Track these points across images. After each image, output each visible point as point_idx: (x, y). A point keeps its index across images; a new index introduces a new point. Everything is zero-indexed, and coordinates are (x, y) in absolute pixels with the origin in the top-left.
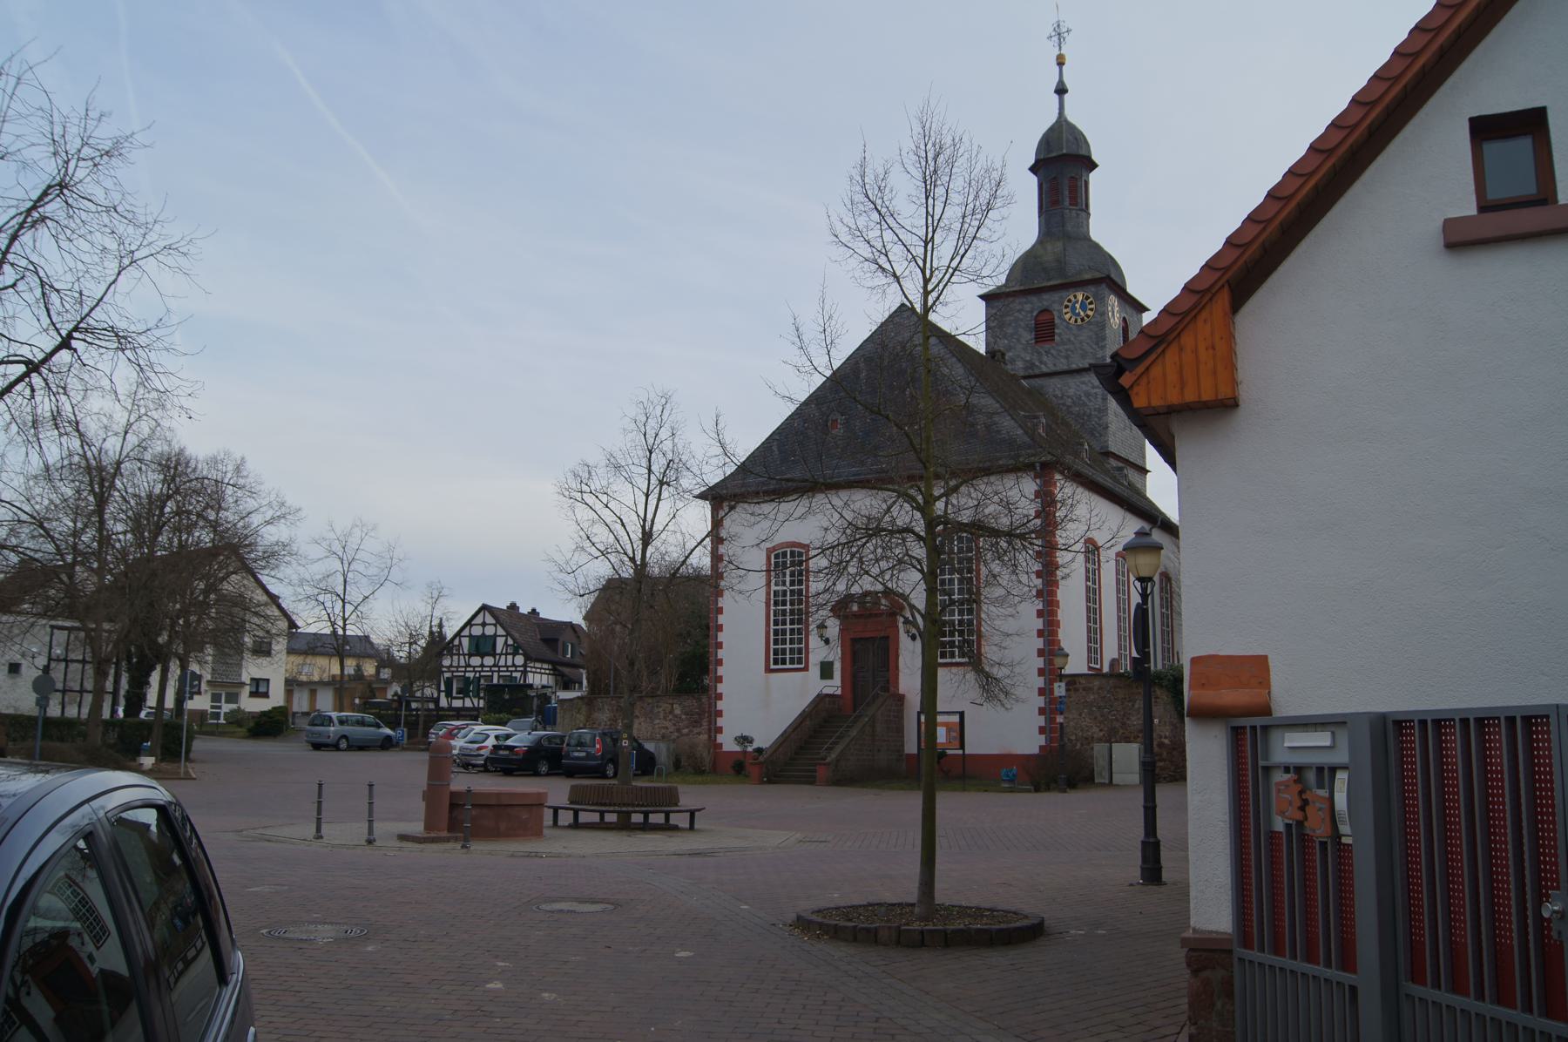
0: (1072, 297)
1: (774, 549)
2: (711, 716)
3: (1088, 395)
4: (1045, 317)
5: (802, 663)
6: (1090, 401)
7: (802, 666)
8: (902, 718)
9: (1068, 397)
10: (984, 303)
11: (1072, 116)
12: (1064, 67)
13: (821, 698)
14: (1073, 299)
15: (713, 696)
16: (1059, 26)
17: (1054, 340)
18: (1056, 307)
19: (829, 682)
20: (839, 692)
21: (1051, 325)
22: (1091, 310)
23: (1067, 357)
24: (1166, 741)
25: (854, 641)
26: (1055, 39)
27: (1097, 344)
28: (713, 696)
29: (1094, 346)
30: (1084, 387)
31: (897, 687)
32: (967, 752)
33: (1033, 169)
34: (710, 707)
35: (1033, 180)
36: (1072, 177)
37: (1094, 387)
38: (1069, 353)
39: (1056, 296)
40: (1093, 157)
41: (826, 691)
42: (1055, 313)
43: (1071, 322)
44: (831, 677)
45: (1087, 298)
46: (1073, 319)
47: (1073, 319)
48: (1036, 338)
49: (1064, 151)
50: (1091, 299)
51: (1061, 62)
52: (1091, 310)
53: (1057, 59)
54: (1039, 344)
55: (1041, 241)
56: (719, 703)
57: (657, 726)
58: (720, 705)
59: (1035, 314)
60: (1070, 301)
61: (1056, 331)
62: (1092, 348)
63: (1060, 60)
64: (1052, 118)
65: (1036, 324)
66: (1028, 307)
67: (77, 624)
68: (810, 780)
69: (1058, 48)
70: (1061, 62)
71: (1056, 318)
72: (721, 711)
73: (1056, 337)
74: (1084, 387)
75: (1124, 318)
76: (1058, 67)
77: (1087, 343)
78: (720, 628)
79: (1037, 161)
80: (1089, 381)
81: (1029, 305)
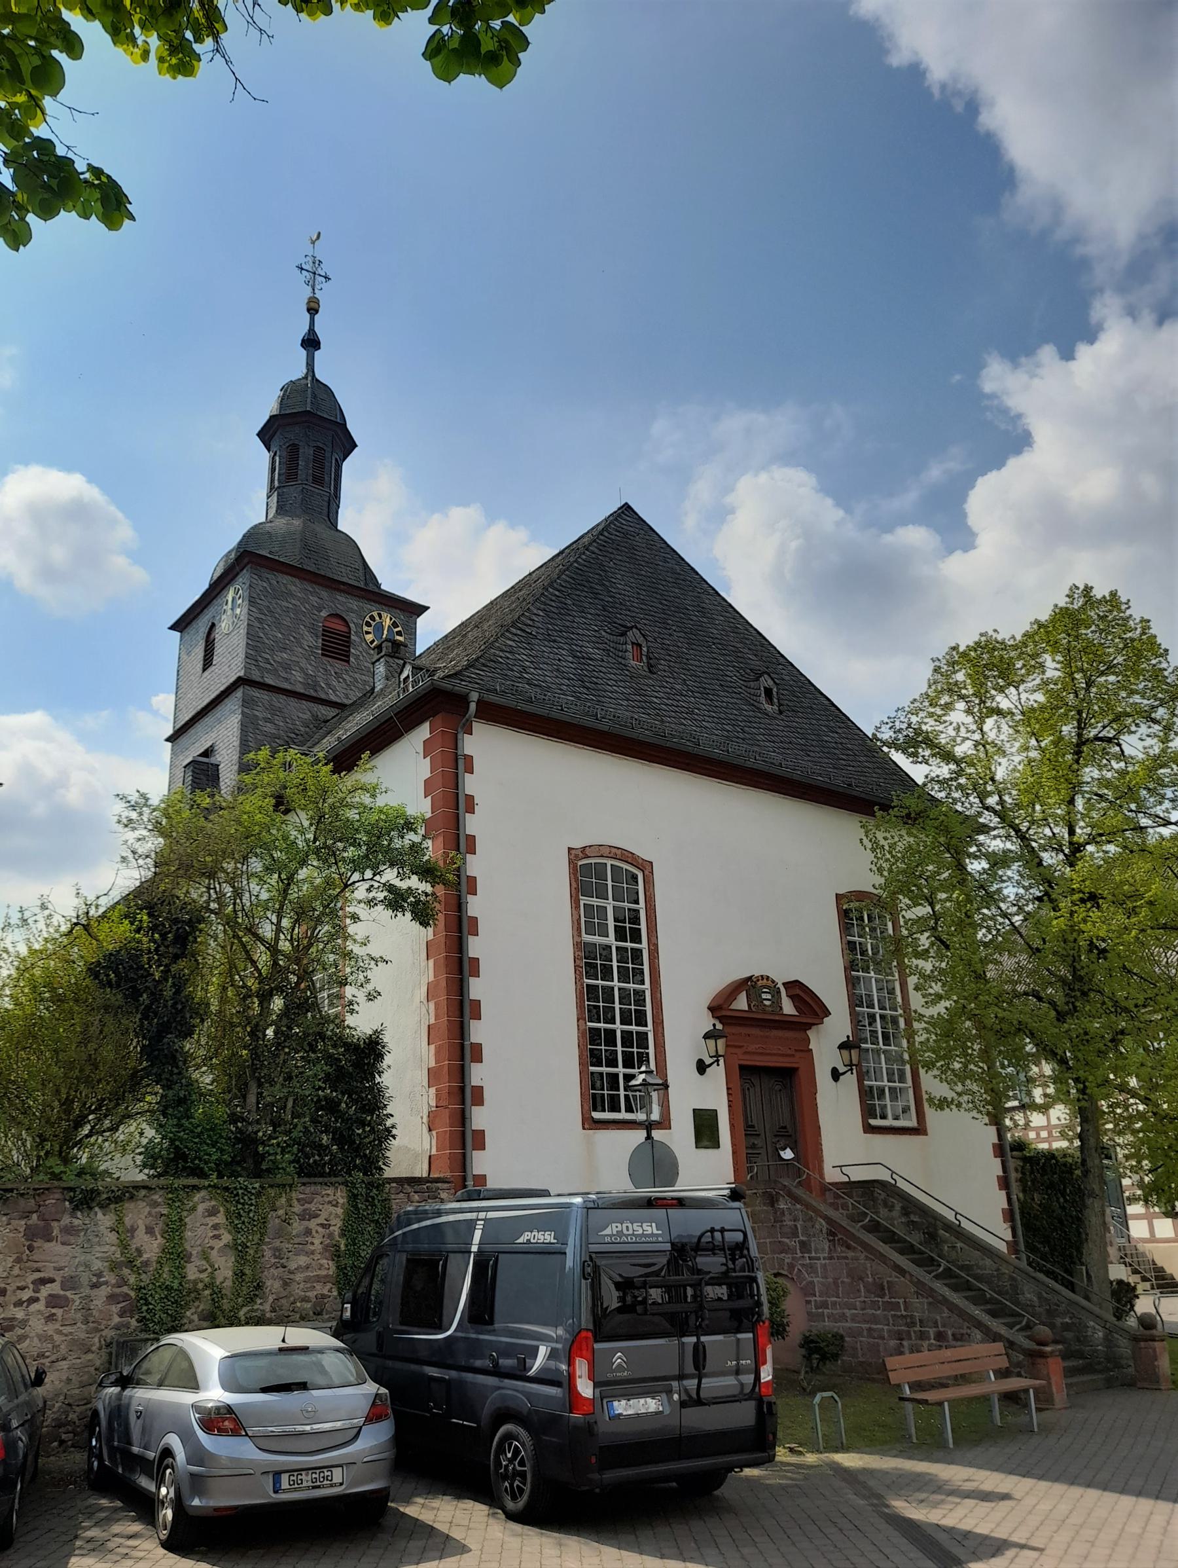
0: (375, 614)
4: (339, 627)
12: (316, 317)
14: (377, 618)
25: (742, 1068)
33: (267, 434)
42: (352, 625)
44: (716, 1144)
50: (399, 629)
51: (313, 309)
53: (309, 303)
57: (299, 1277)
60: (372, 618)
63: (312, 305)
70: (313, 309)
76: (308, 316)
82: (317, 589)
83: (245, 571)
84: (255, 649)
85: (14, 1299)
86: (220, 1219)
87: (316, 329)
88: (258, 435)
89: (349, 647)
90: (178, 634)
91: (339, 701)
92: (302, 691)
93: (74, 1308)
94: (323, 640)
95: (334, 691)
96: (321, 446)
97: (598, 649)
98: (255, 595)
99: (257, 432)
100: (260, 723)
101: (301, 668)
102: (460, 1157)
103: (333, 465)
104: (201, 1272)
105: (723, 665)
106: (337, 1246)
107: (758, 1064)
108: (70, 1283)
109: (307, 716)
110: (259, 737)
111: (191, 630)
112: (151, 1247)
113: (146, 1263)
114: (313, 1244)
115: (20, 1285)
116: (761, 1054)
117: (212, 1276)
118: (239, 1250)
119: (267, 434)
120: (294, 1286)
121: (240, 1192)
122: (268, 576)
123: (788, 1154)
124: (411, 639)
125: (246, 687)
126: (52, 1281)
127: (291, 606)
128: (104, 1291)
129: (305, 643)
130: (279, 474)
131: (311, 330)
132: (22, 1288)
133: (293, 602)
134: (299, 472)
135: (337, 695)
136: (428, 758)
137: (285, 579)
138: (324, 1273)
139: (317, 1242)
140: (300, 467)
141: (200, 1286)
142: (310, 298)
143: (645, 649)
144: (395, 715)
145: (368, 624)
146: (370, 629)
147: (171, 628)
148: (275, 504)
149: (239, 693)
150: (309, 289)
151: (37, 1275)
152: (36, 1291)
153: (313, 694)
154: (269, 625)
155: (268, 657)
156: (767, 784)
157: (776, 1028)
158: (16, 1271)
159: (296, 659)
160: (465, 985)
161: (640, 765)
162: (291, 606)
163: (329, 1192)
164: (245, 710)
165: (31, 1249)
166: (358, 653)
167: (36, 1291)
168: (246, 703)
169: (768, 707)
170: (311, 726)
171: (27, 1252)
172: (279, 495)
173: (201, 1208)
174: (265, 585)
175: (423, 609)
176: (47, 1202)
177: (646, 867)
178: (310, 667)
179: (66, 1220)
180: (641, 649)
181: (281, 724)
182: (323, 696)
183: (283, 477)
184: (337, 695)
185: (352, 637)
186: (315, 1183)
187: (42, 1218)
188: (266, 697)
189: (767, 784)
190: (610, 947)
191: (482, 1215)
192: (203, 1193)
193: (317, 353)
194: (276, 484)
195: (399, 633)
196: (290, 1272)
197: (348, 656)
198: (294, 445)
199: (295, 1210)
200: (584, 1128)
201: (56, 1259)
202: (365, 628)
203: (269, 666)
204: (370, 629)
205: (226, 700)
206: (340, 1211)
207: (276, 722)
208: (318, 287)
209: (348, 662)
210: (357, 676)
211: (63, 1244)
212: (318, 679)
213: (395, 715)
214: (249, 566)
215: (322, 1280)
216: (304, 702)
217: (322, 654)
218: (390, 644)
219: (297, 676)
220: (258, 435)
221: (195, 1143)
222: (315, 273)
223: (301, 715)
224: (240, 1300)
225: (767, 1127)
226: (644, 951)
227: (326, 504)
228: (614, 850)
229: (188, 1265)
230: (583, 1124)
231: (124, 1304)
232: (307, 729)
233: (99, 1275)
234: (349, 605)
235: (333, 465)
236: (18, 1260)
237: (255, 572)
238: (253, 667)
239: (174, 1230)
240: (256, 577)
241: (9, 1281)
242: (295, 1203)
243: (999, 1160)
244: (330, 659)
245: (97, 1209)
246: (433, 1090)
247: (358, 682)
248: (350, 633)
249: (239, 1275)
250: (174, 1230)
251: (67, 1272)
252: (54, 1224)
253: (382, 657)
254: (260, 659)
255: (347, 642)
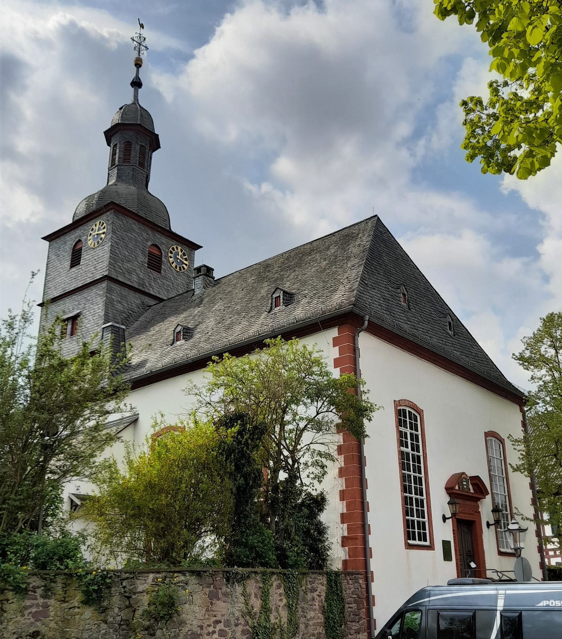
0: (175, 247)
11: (143, 103)
12: (140, 69)
14: (176, 249)
42: (163, 252)
50: (186, 257)
57: (311, 623)
60: (173, 249)
63: (139, 62)
76: (135, 68)
82: (147, 228)
83: (108, 213)
84: (114, 259)
85: (206, 632)
86: (282, 591)
87: (140, 76)
88: (105, 133)
89: (161, 264)
90: (48, 243)
91: (155, 295)
92: (137, 287)
93: (229, 637)
94: (148, 259)
95: (153, 289)
96: (143, 144)
97: (389, 294)
98: (115, 228)
99: (104, 130)
100: (115, 303)
101: (137, 274)
102: (364, 561)
104: (276, 619)
106: (324, 607)
107: (462, 518)
108: (227, 623)
109: (139, 302)
110: (114, 311)
111: (60, 241)
112: (256, 604)
113: (255, 614)
114: (315, 605)
115: (208, 624)
116: (464, 513)
117: (280, 621)
118: (289, 607)
120: (309, 628)
121: (291, 576)
122: (122, 218)
123: (473, 565)
124: (192, 263)
125: (109, 282)
126: (220, 622)
127: (133, 237)
128: (240, 628)
129: (139, 259)
130: (119, 158)
131: (137, 77)
132: (209, 626)
133: (134, 235)
134: (131, 158)
135: (154, 291)
136: (337, 348)
137: (131, 221)
138: (319, 621)
139: (317, 604)
140: (132, 155)
141: (276, 626)
142: (137, 58)
143: (407, 297)
145: (171, 253)
146: (172, 255)
147: (43, 238)
148: (116, 175)
149: (104, 285)
150: (137, 52)
151: (214, 619)
152: (215, 627)
153: (141, 288)
154: (122, 247)
155: (120, 265)
156: (460, 373)
157: (468, 500)
158: (207, 616)
159: (135, 268)
160: (363, 470)
161: (417, 359)
162: (133, 237)
163: (320, 578)
164: (108, 295)
165: (211, 604)
166: (166, 268)
167: (215, 627)
168: (109, 291)
169: (450, 332)
170: (141, 308)
171: (211, 606)
172: (118, 170)
173: (275, 584)
174: (120, 223)
176: (217, 579)
178: (141, 274)
179: (224, 589)
180: (405, 297)
181: (126, 305)
182: (147, 291)
183: (121, 160)
184: (154, 291)
185: (163, 259)
186: (316, 573)
187: (215, 588)
188: (119, 289)
189: (460, 373)
190: (409, 454)
192: (275, 576)
193: (140, 90)
194: (117, 162)
195: (186, 259)
196: (308, 620)
197: (160, 270)
198: (128, 142)
199: (308, 587)
201: (221, 610)
202: (170, 255)
203: (120, 271)
204: (172, 255)
205: (92, 287)
206: (324, 588)
207: (124, 304)
208: (141, 52)
209: (160, 272)
210: (164, 281)
211: (224, 602)
212: (145, 281)
214: (113, 210)
215: (320, 625)
216: (137, 293)
217: (148, 267)
218: (206, 268)
219: (135, 278)
220: (105, 133)
221: (265, 549)
222: (140, 45)
223: (135, 301)
224: (290, 634)
225: (464, 552)
226: (421, 456)
227: (145, 179)
228: (410, 403)
229: (271, 615)
231: (248, 635)
232: (139, 309)
233: (238, 619)
234: (161, 240)
236: (207, 610)
237: (115, 214)
238: (113, 270)
239: (265, 596)
240: (116, 218)
241: (204, 622)
242: (308, 583)
243: (541, 571)
244: (152, 271)
245: (236, 583)
246: (345, 525)
247: (164, 285)
248: (162, 256)
249: (290, 621)
250: (265, 596)
251: (226, 617)
252: (220, 591)
253: (201, 275)
254: (116, 265)
255: (160, 261)
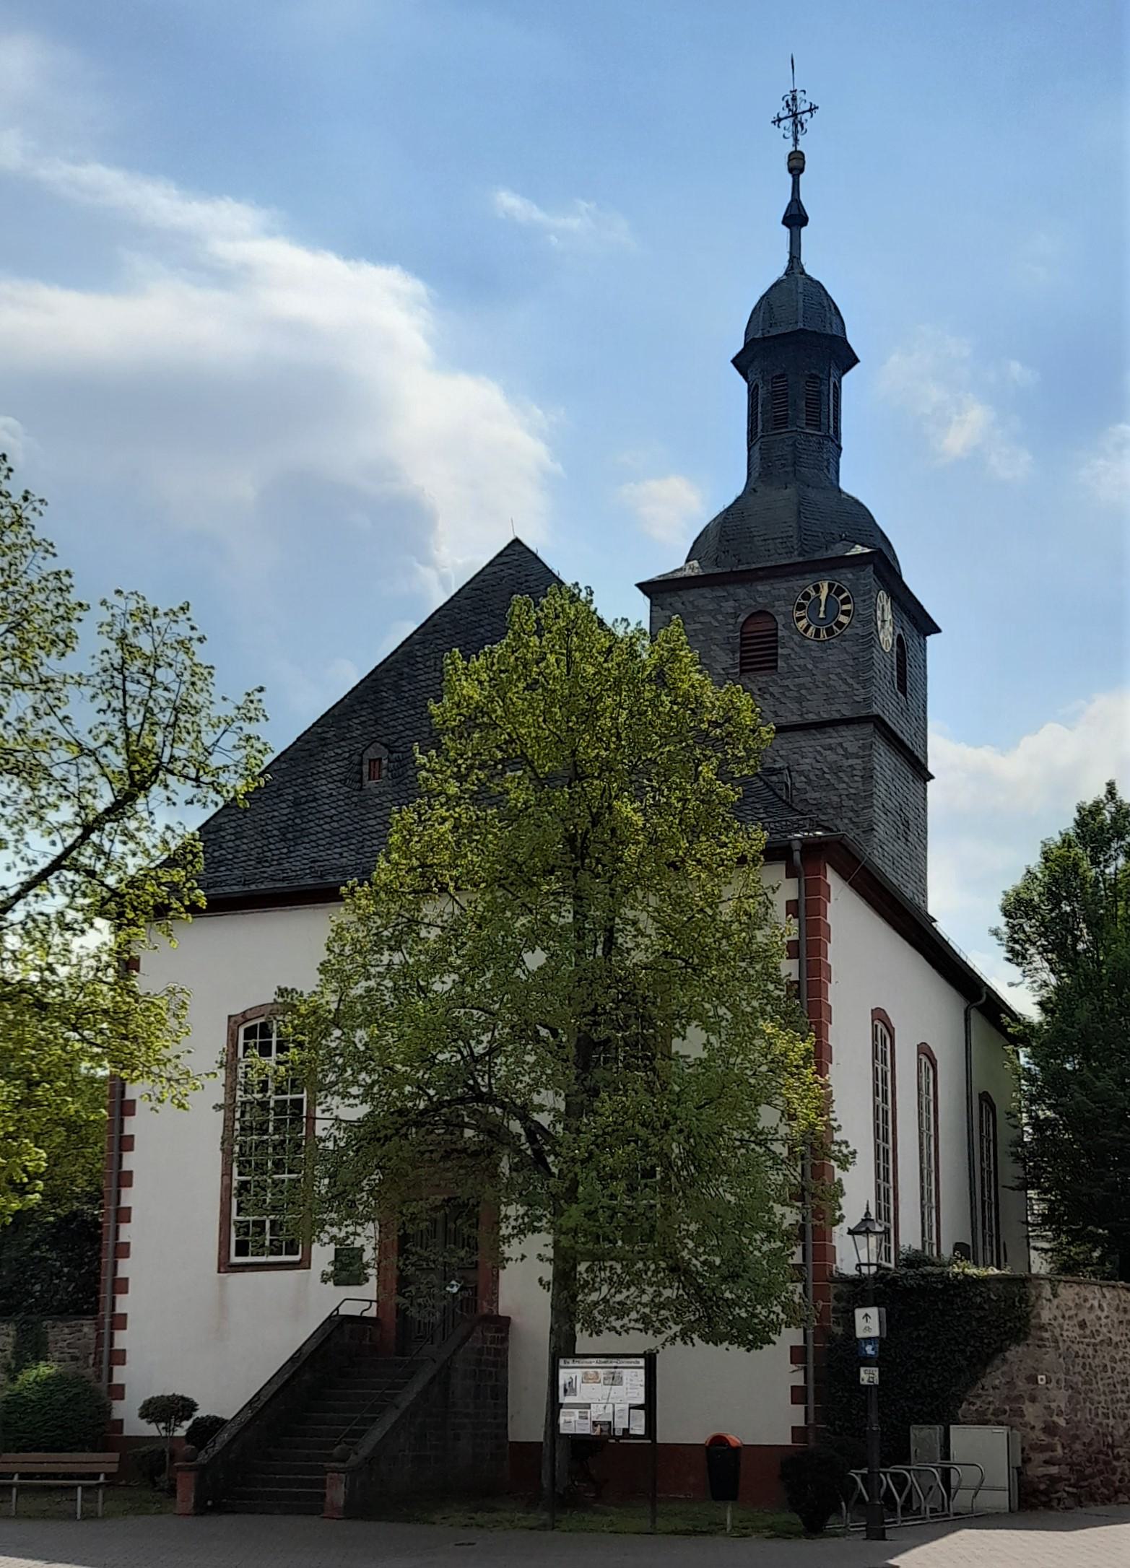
1: (244, 1016)
2: (101, 1362)
3: (836, 770)
4: (760, 626)
5: (297, 1253)
6: (840, 780)
7: (297, 1258)
8: (505, 1366)
9: (801, 773)
10: (647, 601)
11: (813, 266)
12: (802, 176)
13: (337, 1325)
15: (107, 1320)
16: (794, 99)
17: (776, 667)
18: (780, 606)
19: (353, 1291)
20: (372, 1313)
21: (771, 641)
22: (846, 613)
23: (799, 700)
24: (1062, 1422)
26: (787, 123)
27: (856, 676)
28: (107, 1320)
29: (850, 681)
30: (831, 756)
31: (494, 1301)
32: (659, 1440)
33: (740, 362)
34: (99, 1344)
35: (739, 387)
36: (812, 376)
37: (847, 756)
38: (803, 692)
39: (781, 587)
40: (851, 340)
41: (349, 1309)
43: (808, 635)
45: (840, 591)
46: (812, 630)
47: (812, 630)
48: (742, 664)
49: (801, 325)
51: (796, 164)
52: (846, 613)
54: (747, 675)
55: (750, 489)
56: (119, 1335)
58: (122, 1340)
59: (741, 620)
61: (780, 651)
62: (847, 684)
63: (794, 163)
64: (777, 268)
65: (742, 639)
66: (729, 606)
67: (621, 1441)
68: (311, 1504)
69: (791, 141)
71: (780, 627)
72: (122, 1387)
73: (780, 663)
74: (831, 756)
75: (899, 636)
76: (789, 178)
77: (838, 674)
78: (121, 1286)
79: (751, 344)
80: (841, 744)
81: (731, 603)
99: (731, 358)
103: (832, 391)
105: (301, 870)
119: (740, 362)
144: (863, 866)
146: (803, 613)
175: (938, 630)
177: (234, 1022)
191: (234, 1217)
193: (804, 230)
200: (219, 1272)
202: (797, 614)
213: (863, 866)
230: (219, 1269)
235: (832, 391)
